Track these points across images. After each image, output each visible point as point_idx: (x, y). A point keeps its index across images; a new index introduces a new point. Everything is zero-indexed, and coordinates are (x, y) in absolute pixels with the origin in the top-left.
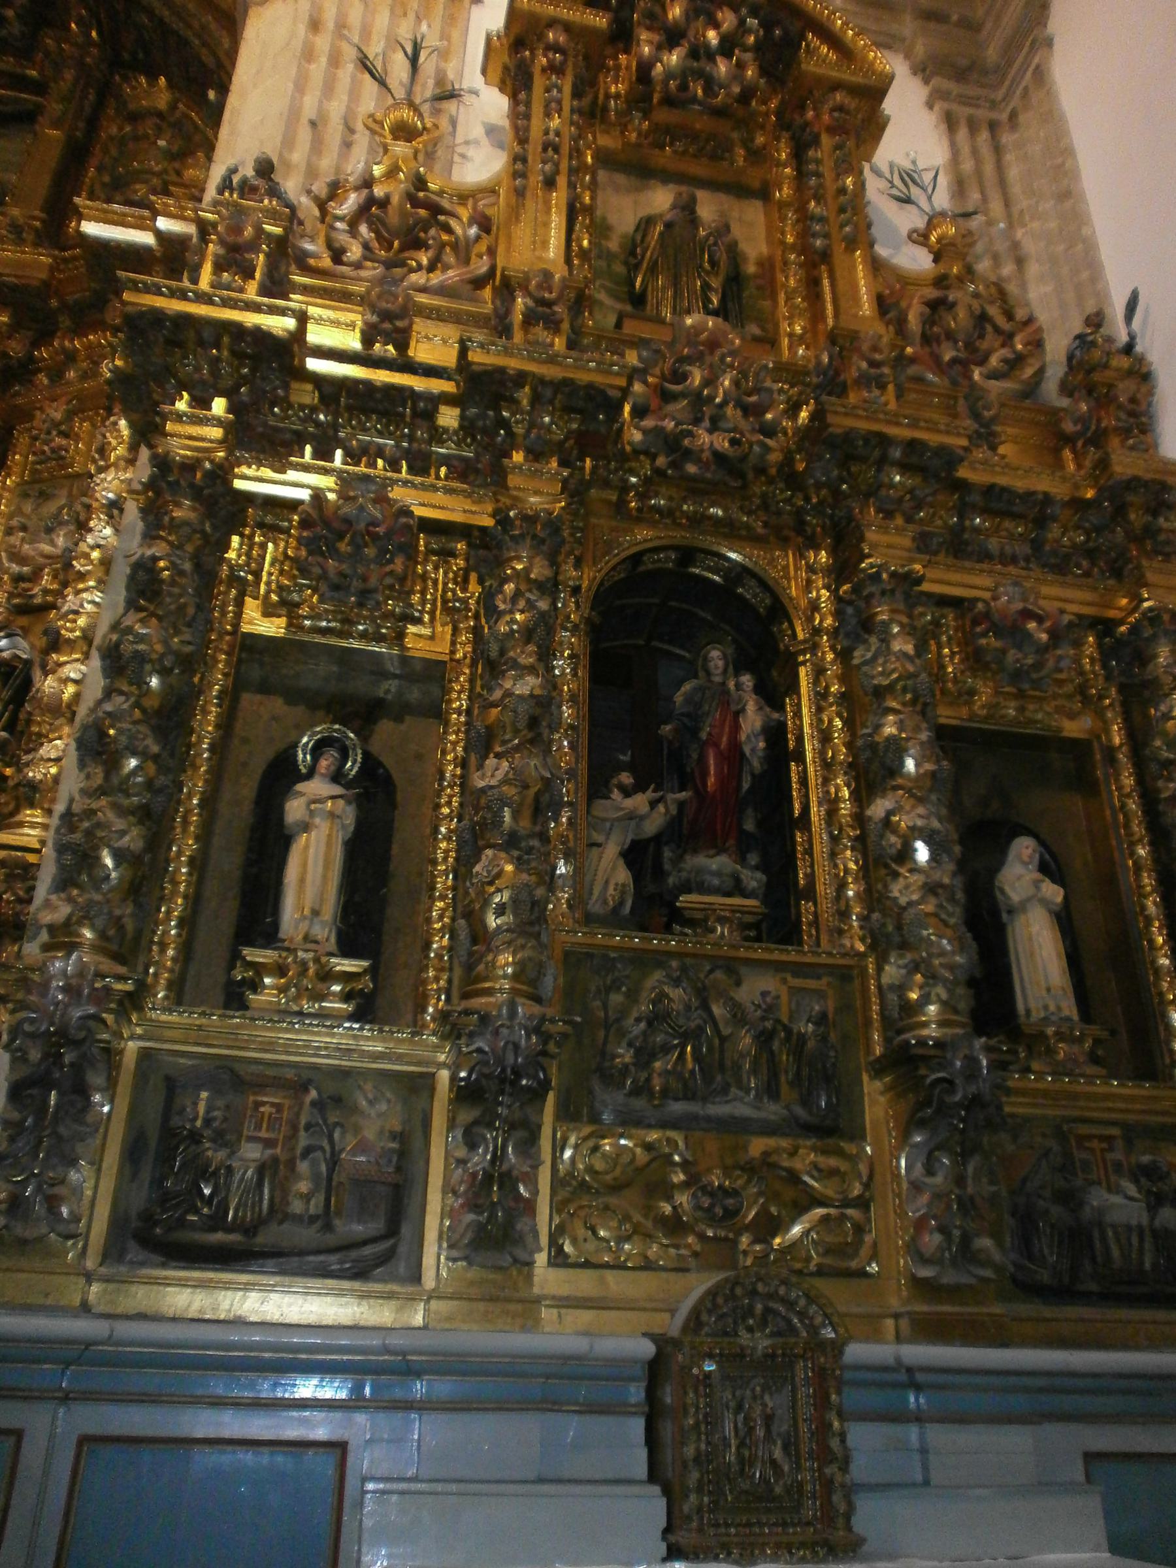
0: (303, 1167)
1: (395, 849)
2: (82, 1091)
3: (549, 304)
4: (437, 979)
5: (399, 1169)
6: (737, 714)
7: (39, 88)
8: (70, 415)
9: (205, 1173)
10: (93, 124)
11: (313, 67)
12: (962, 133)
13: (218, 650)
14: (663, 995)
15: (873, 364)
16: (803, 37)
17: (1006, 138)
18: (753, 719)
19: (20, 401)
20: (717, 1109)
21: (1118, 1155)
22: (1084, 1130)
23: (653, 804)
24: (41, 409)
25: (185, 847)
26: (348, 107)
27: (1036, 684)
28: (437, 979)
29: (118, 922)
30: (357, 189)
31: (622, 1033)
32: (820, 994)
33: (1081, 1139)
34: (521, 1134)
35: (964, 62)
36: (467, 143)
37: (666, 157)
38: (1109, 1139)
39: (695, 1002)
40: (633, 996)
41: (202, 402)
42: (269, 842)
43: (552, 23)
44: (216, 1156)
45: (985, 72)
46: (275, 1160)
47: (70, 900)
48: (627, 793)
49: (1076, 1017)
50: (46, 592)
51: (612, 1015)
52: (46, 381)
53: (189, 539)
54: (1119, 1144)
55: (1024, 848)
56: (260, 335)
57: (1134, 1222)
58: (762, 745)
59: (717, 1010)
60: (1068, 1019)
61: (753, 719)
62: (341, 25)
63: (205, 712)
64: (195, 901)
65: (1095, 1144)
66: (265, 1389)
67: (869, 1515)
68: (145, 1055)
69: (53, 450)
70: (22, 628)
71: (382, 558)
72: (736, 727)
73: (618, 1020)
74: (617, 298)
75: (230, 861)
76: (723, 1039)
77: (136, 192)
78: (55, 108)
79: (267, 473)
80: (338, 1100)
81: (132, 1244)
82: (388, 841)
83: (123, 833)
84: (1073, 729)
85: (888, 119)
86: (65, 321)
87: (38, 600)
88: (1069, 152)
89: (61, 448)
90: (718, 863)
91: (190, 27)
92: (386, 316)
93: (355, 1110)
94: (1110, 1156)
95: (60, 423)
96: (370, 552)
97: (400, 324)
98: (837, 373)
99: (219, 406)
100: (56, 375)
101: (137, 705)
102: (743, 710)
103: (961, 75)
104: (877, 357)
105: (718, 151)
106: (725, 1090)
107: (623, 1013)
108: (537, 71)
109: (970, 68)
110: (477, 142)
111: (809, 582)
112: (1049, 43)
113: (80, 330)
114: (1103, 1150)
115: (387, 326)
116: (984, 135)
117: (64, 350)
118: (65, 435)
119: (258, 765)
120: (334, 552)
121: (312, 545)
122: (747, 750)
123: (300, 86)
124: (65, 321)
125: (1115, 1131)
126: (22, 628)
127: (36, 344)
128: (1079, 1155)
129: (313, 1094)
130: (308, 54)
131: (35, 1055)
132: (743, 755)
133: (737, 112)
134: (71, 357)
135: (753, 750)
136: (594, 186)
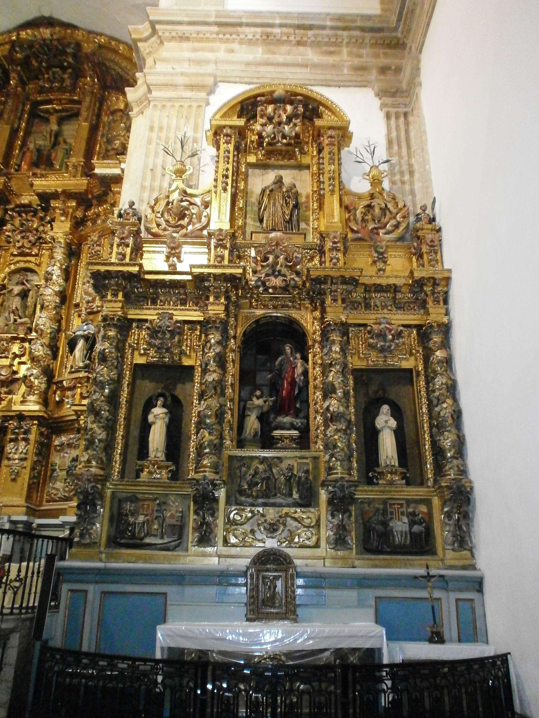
0: (156, 522)
1: (183, 425)
2: (94, 505)
3: (222, 240)
4: (192, 466)
5: (181, 521)
6: (294, 368)
7: (79, 102)
8: (100, 237)
9: (129, 525)
10: (99, 116)
11: (151, 146)
12: (393, 120)
13: (127, 370)
14: (257, 467)
15: (335, 243)
16: (319, 108)
17: (411, 119)
18: (299, 370)
19: (83, 233)
20: (272, 501)
21: (404, 509)
22: (393, 502)
23: (265, 402)
24: (89, 236)
25: (120, 433)
26: (163, 160)
27: (391, 352)
28: (192, 466)
29: (101, 459)
30: (164, 199)
31: (245, 479)
32: (308, 464)
33: (391, 505)
34: (210, 512)
35: (393, 90)
36: (204, 165)
37: (272, 161)
38: (401, 505)
39: (267, 469)
40: (249, 468)
41: (115, 295)
42: (146, 427)
43: (224, 127)
44: (131, 520)
45: (402, 92)
46: (148, 520)
47: (88, 454)
48: (258, 398)
49: (397, 464)
50: (97, 307)
51: (242, 474)
52: (91, 225)
53: (113, 342)
54: (405, 505)
55: (385, 408)
56: (130, 274)
57: (404, 530)
58: (302, 378)
59: (274, 471)
60: (394, 466)
61: (299, 370)
62: (161, 129)
63: (124, 391)
64: (126, 447)
65: (396, 506)
66: (233, 581)
67: (299, 611)
68: (113, 493)
69: (95, 252)
70: (91, 320)
71: (172, 337)
72: (294, 373)
73: (244, 475)
74: (255, 221)
75: (135, 432)
76: (276, 480)
77: (115, 144)
78: (84, 113)
79: (137, 312)
80: (164, 503)
81: (112, 544)
82: (181, 421)
83: (100, 434)
84: (405, 365)
85: (352, 133)
86: (95, 202)
87: (95, 310)
88: (425, 132)
89: (98, 251)
90: (287, 420)
91: (128, 74)
92: (173, 248)
93: (169, 505)
94: (400, 510)
95: (97, 241)
96: (168, 336)
97: (177, 251)
98: (323, 247)
99: (120, 294)
100: (94, 222)
101: (102, 395)
102: (296, 366)
103: (393, 95)
104: (336, 240)
105: (291, 156)
106: (275, 495)
107: (246, 473)
108: (221, 143)
109: (396, 92)
110: (208, 164)
111: (313, 323)
112: (420, 84)
113: (100, 204)
114: (398, 508)
115: (173, 252)
116: (402, 119)
117: (95, 212)
118: (99, 245)
119: (143, 402)
120: (157, 337)
121: (151, 336)
122: (297, 380)
123: (147, 156)
124: (95, 202)
125: (404, 502)
126: (91, 320)
127: (86, 211)
128: (389, 510)
129: (158, 501)
130: (149, 142)
131: (81, 497)
132: (296, 382)
133: (297, 141)
134: (98, 215)
135: (300, 380)
136: (246, 180)
